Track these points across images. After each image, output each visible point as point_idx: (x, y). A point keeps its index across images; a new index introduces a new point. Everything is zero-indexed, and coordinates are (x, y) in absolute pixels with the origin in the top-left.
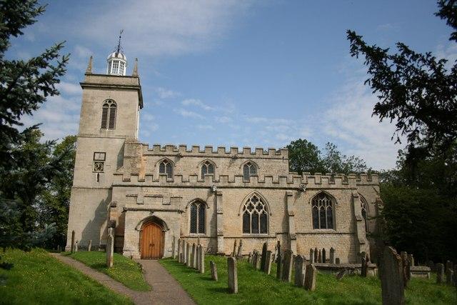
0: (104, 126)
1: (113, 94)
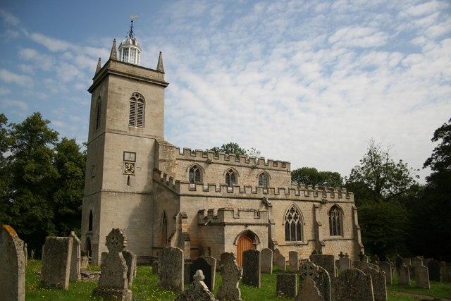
0: (132, 123)
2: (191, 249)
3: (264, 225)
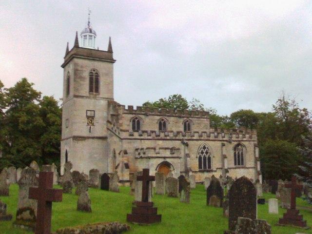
2: (130, 174)
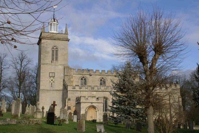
0: (53, 59)
1: (57, 43)
3: (101, 103)
